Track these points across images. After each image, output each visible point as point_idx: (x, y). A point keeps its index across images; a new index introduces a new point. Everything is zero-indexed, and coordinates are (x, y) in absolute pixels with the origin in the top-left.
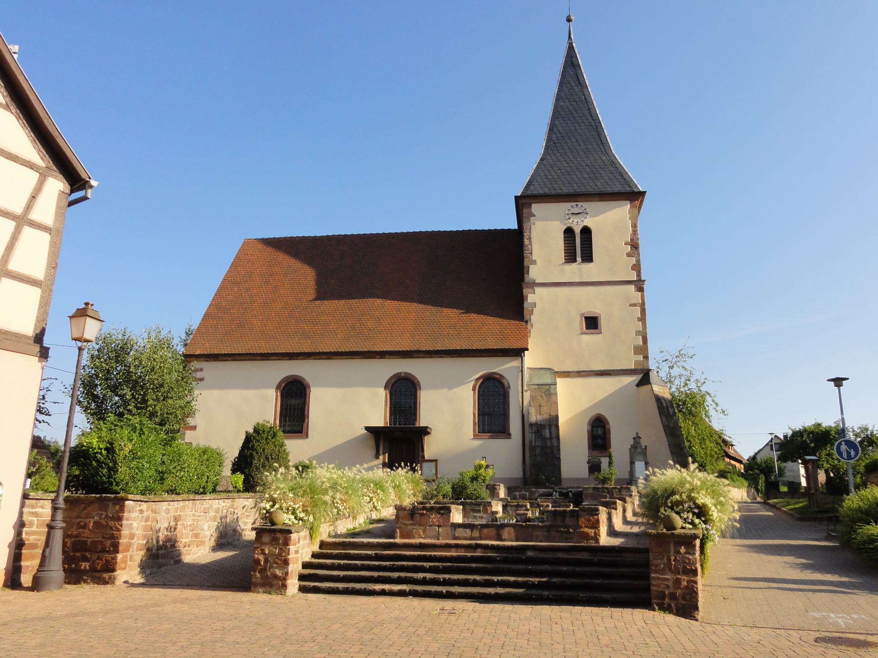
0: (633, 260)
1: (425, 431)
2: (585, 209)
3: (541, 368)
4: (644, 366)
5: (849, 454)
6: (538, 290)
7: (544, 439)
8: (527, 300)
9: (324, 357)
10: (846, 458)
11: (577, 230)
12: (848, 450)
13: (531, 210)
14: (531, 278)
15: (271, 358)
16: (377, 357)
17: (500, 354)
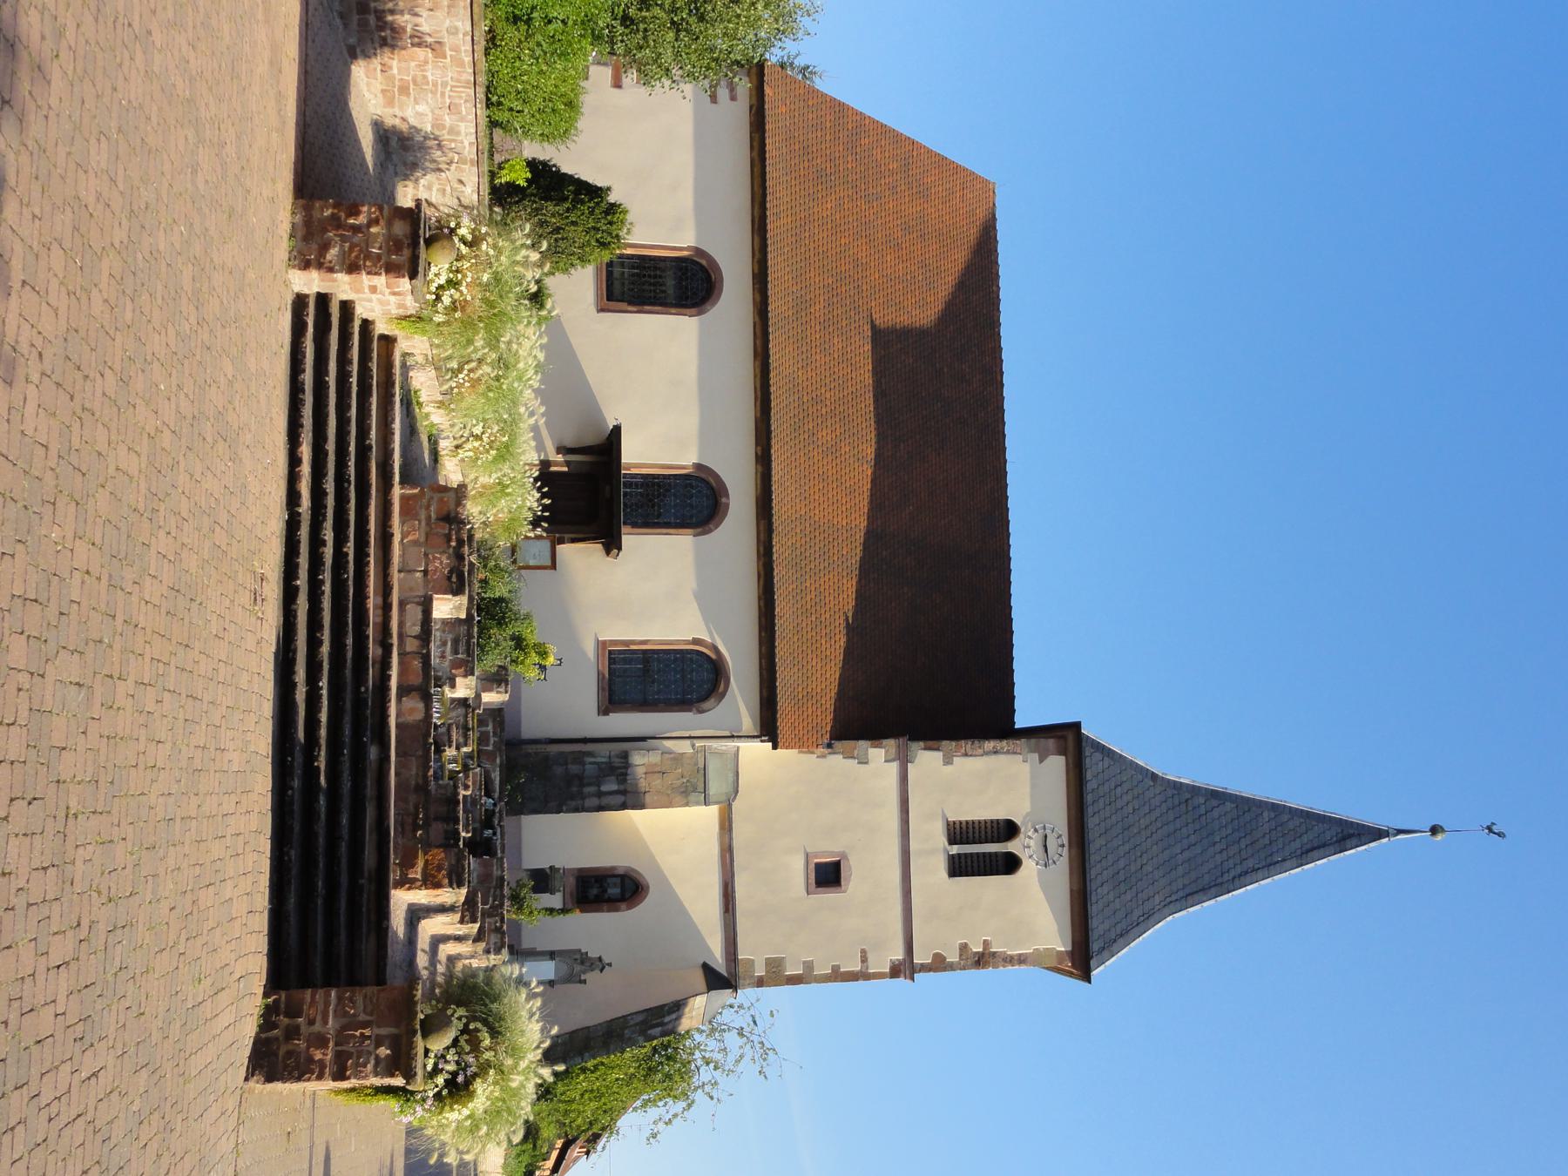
1: (612, 544)
6: (894, 767)
9: (758, 342)
11: (1012, 847)
17: (765, 694)
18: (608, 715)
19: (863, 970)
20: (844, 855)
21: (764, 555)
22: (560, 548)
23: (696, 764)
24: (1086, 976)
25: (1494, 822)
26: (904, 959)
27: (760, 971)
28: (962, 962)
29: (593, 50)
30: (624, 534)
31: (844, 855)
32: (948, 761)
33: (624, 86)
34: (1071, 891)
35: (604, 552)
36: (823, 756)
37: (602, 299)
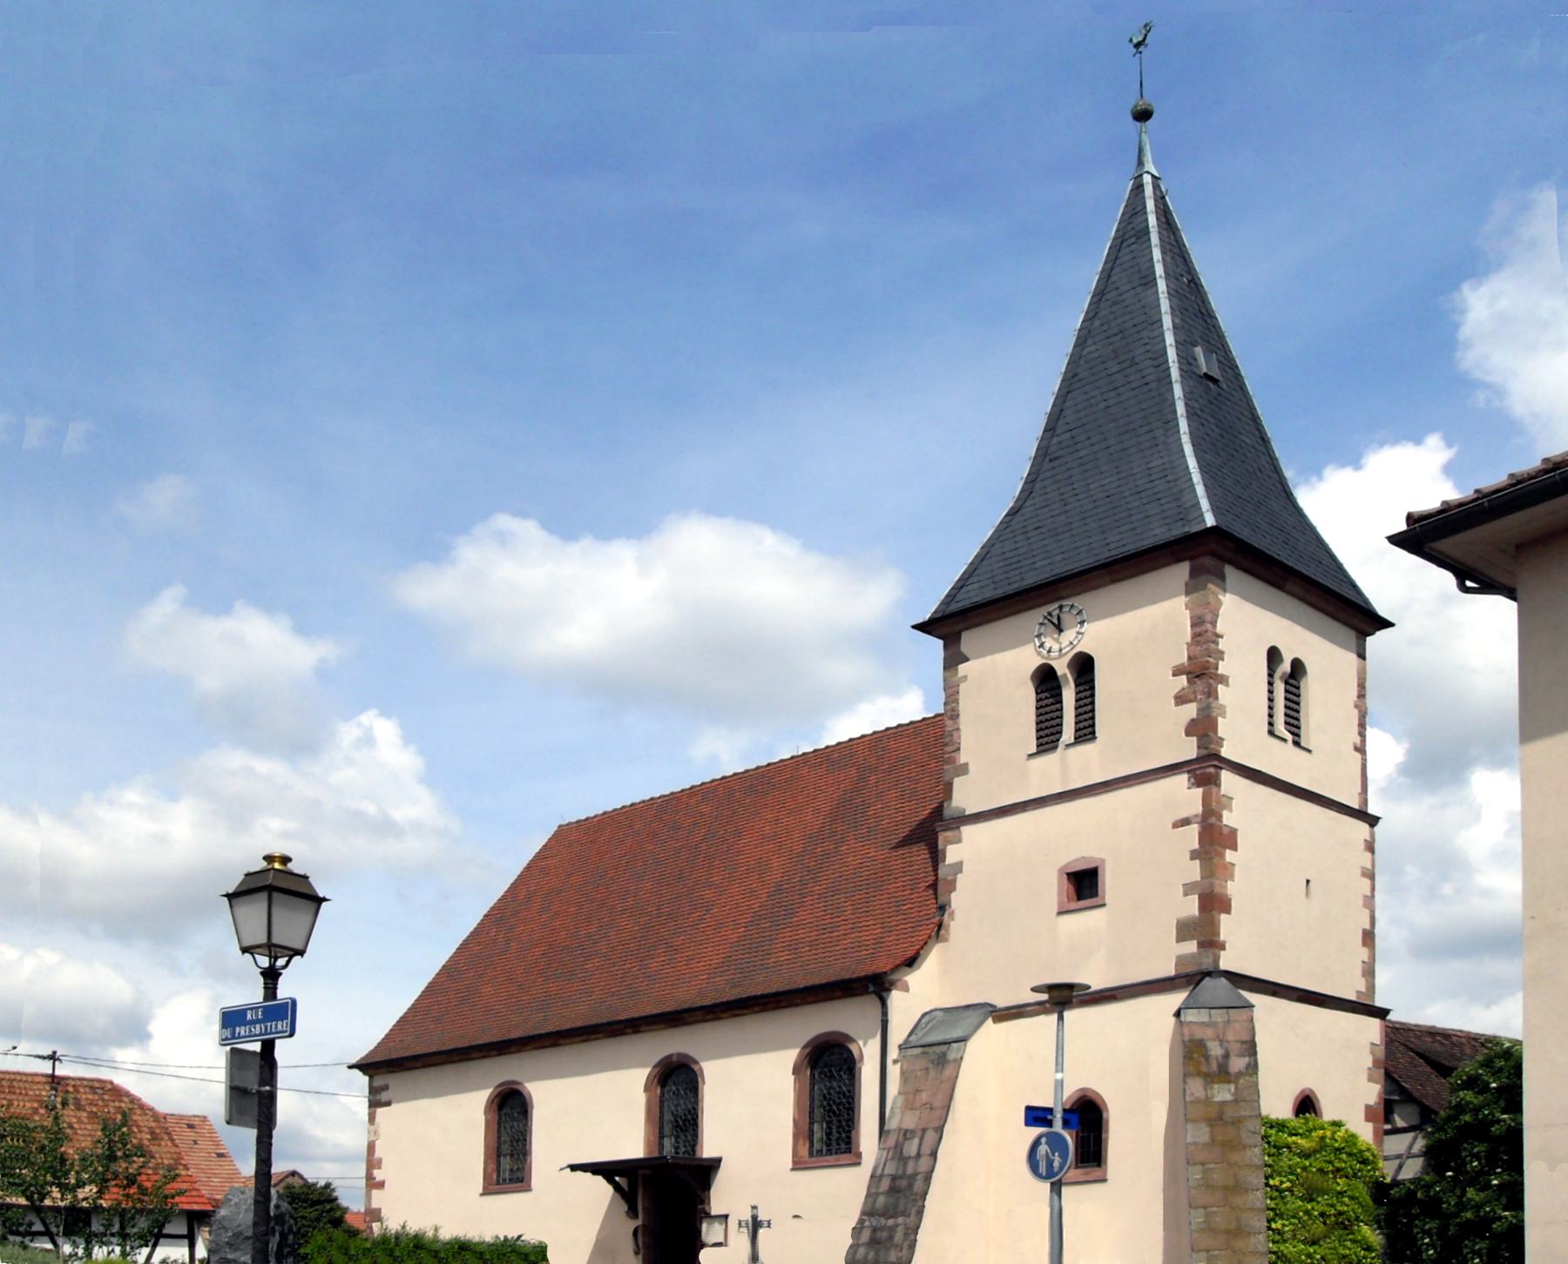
0: (1190, 711)
1: (714, 1165)
2: (1041, 624)
3: (968, 1007)
4: (1201, 964)
5: (1050, 1163)
6: (967, 831)
7: (903, 1159)
8: (944, 861)
9: (547, 1044)
10: (1044, 1174)
11: (1062, 668)
12: (1050, 1155)
13: (959, 648)
14: (957, 808)
15: (473, 1056)
16: (628, 1031)
17: (839, 993)
18: (861, 1153)
19: (1199, 820)
20: (1103, 861)
21: (714, 1013)
22: (713, 1213)
23: (917, 1056)
24: (319, 901)
25: (1128, 39)
26: (1189, 772)
27: (1191, 947)
28: (1199, 697)
29: (277, 1207)
30: (362, 1188)
31: (1103, 861)
32: (964, 770)
33: (1369, 1045)
34: (1113, 582)
35: (722, 1163)
36: (952, 914)
37: (522, 1187)
